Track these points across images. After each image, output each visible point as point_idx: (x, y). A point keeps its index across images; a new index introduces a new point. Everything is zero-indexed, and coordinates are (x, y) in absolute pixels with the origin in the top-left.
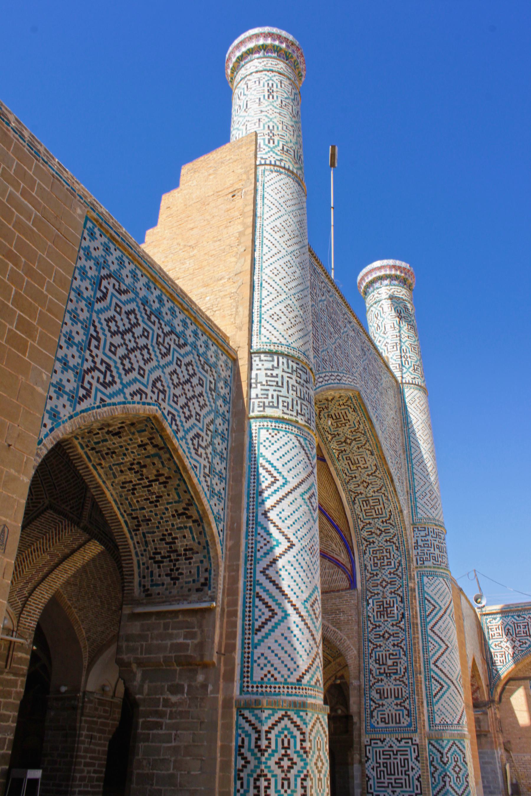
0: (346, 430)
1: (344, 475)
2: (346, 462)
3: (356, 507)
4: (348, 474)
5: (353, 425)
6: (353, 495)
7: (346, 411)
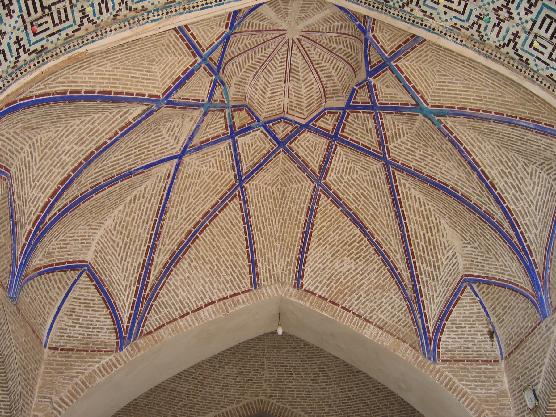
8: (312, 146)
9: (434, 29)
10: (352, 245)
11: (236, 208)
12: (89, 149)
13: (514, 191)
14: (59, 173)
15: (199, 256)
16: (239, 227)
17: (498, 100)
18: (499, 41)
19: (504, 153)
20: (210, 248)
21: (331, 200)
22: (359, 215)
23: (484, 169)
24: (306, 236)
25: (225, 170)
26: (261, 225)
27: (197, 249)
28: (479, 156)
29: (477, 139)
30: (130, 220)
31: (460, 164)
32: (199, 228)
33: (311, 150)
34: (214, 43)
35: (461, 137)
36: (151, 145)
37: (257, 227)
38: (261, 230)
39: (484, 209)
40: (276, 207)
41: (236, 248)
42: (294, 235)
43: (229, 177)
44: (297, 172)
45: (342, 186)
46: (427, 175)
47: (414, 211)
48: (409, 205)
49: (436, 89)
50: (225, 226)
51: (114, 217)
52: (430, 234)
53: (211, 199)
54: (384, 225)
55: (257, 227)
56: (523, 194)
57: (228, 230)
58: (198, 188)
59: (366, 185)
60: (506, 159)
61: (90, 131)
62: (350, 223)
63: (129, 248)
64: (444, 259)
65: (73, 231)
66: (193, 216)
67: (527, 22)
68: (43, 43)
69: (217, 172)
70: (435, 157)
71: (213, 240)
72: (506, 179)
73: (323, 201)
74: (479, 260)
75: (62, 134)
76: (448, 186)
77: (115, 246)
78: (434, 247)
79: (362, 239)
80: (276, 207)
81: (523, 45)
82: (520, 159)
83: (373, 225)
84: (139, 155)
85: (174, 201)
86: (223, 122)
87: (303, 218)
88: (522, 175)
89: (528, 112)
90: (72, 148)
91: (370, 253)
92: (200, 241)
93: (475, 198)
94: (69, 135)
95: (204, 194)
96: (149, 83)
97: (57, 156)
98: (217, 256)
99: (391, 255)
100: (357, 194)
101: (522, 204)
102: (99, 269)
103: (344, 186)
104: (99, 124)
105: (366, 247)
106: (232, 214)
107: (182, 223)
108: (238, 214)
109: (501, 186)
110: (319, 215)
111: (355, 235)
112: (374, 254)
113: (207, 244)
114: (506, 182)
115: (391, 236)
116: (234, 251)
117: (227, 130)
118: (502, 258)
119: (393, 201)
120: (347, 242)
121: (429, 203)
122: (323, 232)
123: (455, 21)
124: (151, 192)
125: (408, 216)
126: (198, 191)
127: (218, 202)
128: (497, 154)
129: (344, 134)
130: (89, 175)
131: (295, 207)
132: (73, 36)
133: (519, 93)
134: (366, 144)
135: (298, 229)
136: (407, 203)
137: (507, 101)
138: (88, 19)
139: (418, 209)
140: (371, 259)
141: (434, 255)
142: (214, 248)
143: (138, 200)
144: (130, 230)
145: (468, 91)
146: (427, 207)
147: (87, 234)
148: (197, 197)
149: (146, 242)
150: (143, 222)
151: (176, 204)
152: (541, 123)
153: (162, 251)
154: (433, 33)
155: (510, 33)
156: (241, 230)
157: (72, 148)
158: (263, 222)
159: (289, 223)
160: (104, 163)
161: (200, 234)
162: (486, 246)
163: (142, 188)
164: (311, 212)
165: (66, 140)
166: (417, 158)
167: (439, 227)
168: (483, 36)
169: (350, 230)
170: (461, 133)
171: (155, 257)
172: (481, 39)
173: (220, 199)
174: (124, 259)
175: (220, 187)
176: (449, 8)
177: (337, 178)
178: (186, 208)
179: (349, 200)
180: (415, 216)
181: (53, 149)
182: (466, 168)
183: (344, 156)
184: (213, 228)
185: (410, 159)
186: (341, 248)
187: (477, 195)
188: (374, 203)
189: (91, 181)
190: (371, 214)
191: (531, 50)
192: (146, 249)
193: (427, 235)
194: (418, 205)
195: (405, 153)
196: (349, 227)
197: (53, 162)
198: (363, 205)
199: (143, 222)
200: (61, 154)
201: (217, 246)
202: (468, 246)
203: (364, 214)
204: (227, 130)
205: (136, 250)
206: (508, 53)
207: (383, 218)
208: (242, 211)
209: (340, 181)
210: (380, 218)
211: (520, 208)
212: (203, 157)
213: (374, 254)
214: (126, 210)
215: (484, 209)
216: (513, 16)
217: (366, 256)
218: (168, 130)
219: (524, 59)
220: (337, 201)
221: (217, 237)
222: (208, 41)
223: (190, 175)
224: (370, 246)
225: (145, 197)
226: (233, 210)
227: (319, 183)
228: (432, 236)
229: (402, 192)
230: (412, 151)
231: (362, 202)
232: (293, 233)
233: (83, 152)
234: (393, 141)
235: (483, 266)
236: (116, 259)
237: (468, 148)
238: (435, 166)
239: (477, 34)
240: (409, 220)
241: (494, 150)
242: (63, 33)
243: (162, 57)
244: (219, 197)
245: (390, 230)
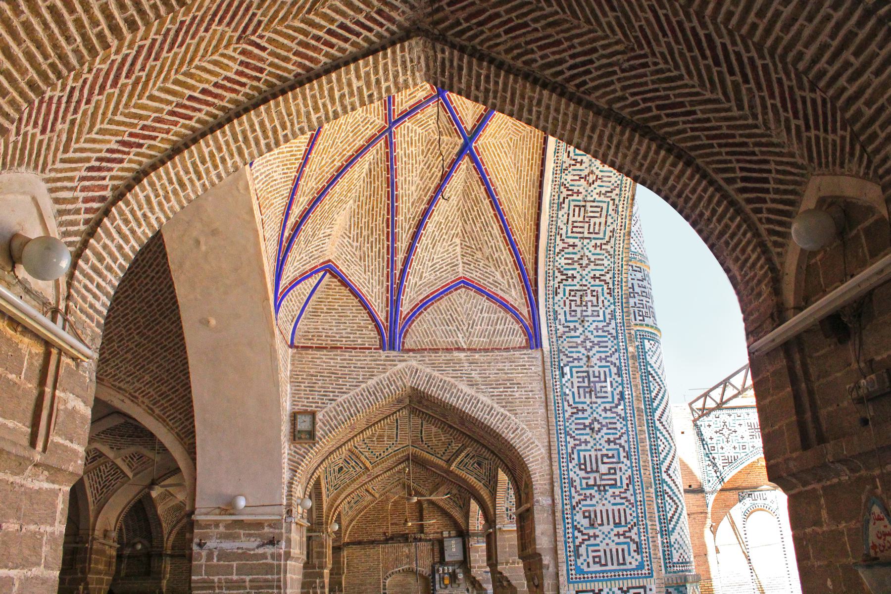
3: (560, 213)
6: (565, 193)
31: (426, 190)
81: (573, 200)
88: (446, 238)
187: (405, 218)
191: (572, 208)
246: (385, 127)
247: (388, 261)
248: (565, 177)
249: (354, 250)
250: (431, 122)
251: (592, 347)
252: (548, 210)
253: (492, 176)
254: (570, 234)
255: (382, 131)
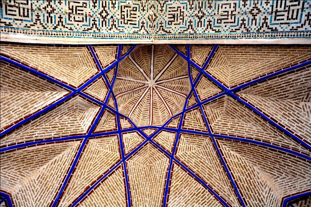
0: (188, 14)
1: (237, 31)
2: (223, 25)
3: (280, 29)
4: (237, 28)
5: (185, 5)
6: (265, 28)
7: (168, 6)
8: (166, 138)
9: (222, 37)
10: (198, 195)
11: (120, 174)
12: (29, 112)
13: (296, 124)
14: (6, 121)
15: (92, 203)
16: (121, 187)
17: (267, 65)
18: (257, 27)
19: (281, 103)
20: (100, 198)
21: (181, 167)
22: (200, 175)
23: (272, 117)
24: (167, 191)
25: (114, 152)
26: (136, 187)
27: (91, 199)
28: (267, 110)
29: (262, 100)
30: (50, 174)
31: (256, 120)
32: (95, 185)
33: (166, 140)
34: (108, 65)
35: (252, 102)
36: (69, 125)
37: (133, 187)
38: (136, 190)
39: (280, 145)
40: (146, 176)
41: (119, 199)
42: (159, 191)
43: (116, 155)
44: (159, 154)
45: (186, 158)
46: (238, 136)
47: (235, 165)
48: (231, 161)
49: (231, 76)
50: (112, 185)
51: (40, 171)
52: (249, 178)
53: (104, 168)
54: (217, 179)
55: (133, 187)
56: (303, 123)
57: (114, 188)
58: (97, 160)
59: (201, 155)
60: (284, 106)
61: (32, 101)
62: (195, 181)
63: (44, 193)
64: (264, 194)
65: (6, 170)
66: (92, 177)
67: (268, 8)
68: (11, 21)
69: (109, 152)
70: (240, 123)
71: (103, 193)
72: (288, 118)
73: (176, 168)
74: (290, 185)
75: (14, 98)
76: (253, 139)
77: (35, 190)
78: (255, 186)
79: (204, 191)
80: (146, 176)
82: (293, 102)
83: (210, 181)
84: (61, 129)
85: (80, 166)
86: (114, 122)
87: (163, 180)
88: (297, 111)
89: (287, 62)
90: (19, 108)
91: (211, 199)
92: (94, 193)
93: (273, 140)
94: (19, 100)
95: (100, 165)
96: (71, 78)
97: (7, 110)
98: (105, 204)
99: (227, 199)
100: (197, 161)
101: (305, 129)
102: (17, 201)
103: (188, 158)
104: (38, 98)
105: (208, 195)
106: (117, 178)
107: (83, 181)
108: (121, 178)
109: (286, 123)
110: (174, 177)
111: (199, 189)
112: (214, 200)
113: (99, 196)
114: (289, 120)
115: (223, 186)
116: (117, 201)
117: (116, 128)
118: (307, 175)
119: (220, 161)
120: (195, 194)
121: (243, 158)
122: (177, 189)
123: (231, 28)
124: (66, 158)
125: (232, 168)
126: (96, 162)
127: (108, 170)
128: (277, 105)
129: (184, 127)
130: (26, 132)
131: (158, 174)
132: (30, 27)
133: (278, 53)
134: (198, 129)
135: (161, 187)
136: (229, 160)
137: (273, 63)
138: (40, 22)
139: (237, 163)
140: (213, 203)
141: (257, 192)
142: (103, 198)
143: (57, 163)
144: (48, 181)
145: (249, 69)
146: (243, 161)
147: (16, 177)
148: (96, 166)
149: (56, 189)
150: (58, 177)
151: (81, 168)
152: (298, 64)
153: (67, 198)
154: (222, 39)
155: (262, 19)
156: (122, 188)
157: (19, 108)
158: (137, 185)
159: (155, 185)
160: (38, 127)
161: (95, 189)
162: (291, 172)
163: (61, 155)
164: (169, 176)
165: (16, 102)
166: (229, 128)
167: (254, 173)
168: (248, 29)
169: (196, 186)
170: (252, 99)
171: (62, 200)
172: (248, 31)
173: (110, 168)
174: (38, 199)
175: (111, 161)
176: (227, 23)
177: (183, 153)
178: (88, 172)
179: (192, 166)
180: (237, 167)
181: (6, 105)
182: (261, 122)
183: (186, 141)
184: (104, 186)
185: (225, 130)
186: (191, 197)
187: (273, 137)
188: (208, 166)
189: (27, 137)
190: (208, 173)
191: (277, 22)
192: (55, 194)
193: (247, 179)
194: (237, 160)
195: (222, 127)
196: (194, 184)
197: (4, 114)
198: (202, 168)
199: (58, 177)
200: (11, 110)
201: (106, 198)
202: (278, 179)
203: (203, 174)
204: (116, 128)
205: (48, 194)
206: (264, 31)
207: (216, 174)
208: (124, 176)
209: (185, 155)
210: (214, 175)
211: (305, 132)
212: (101, 142)
213: (214, 200)
214: (48, 168)
215: (280, 145)
216: (260, 10)
217: (209, 201)
218: (81, 118)
219: (274, 29)
220: (185, 168)
221: (106, 192)
222: (106, 63)
223: (92, 151)
224: (210, 195)
225: (62, 161)
226: (118, 176)
227: (173, 158)
228: (251, 179)
229: (225, 153)
230: (225, 124)
231: (201, 166)
232: (158, 190)
233: (25, 113)
234: (214, 122)
235: (295, 187)
236: (33, 199)
237: (258, 107)
238: (241, 129)
239: (245, 29)
240: (233, 170)
241: (274, 103)
242: (24, 23)
243: (80, 65)
244: (109, 167)
245: (222, 182)
246: (210, 138)
247: (300, 159)
248: (253, 29)
249: (287, 178)
250: (216, 112)
251: (258, 9)
252: (277, 40)
253: (251, 78)
254: (298, 20)
255: (212, 140)
